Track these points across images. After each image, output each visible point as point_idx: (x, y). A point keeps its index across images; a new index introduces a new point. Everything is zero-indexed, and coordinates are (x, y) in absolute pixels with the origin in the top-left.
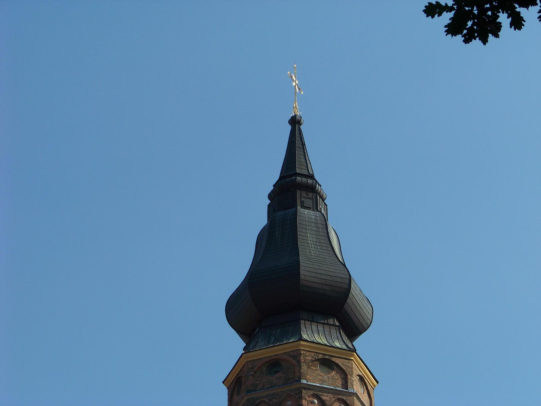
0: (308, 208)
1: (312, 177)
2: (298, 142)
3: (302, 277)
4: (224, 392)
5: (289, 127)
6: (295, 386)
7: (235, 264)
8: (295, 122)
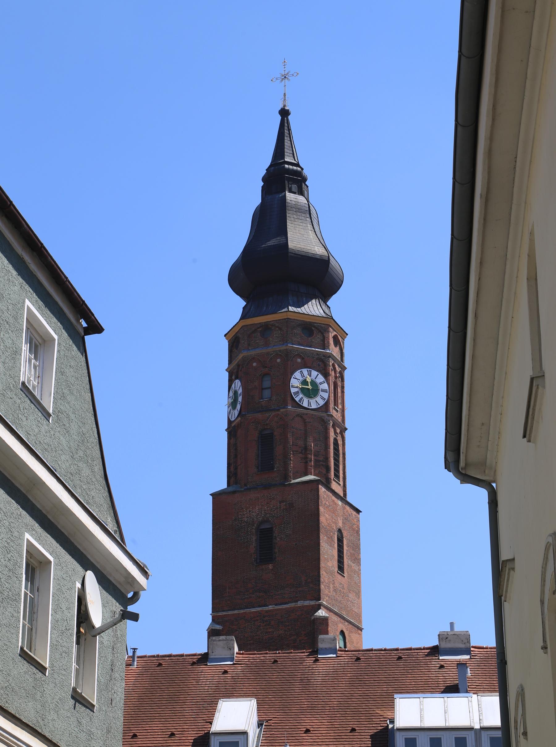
0: (294, 193)
1: (298, 165)
2: (287, 143)
3: (290, 246)
4: (225, 344)
5: (279, 118)
6: (317, 603)
7: (236, 238)
8: (284, 113)
